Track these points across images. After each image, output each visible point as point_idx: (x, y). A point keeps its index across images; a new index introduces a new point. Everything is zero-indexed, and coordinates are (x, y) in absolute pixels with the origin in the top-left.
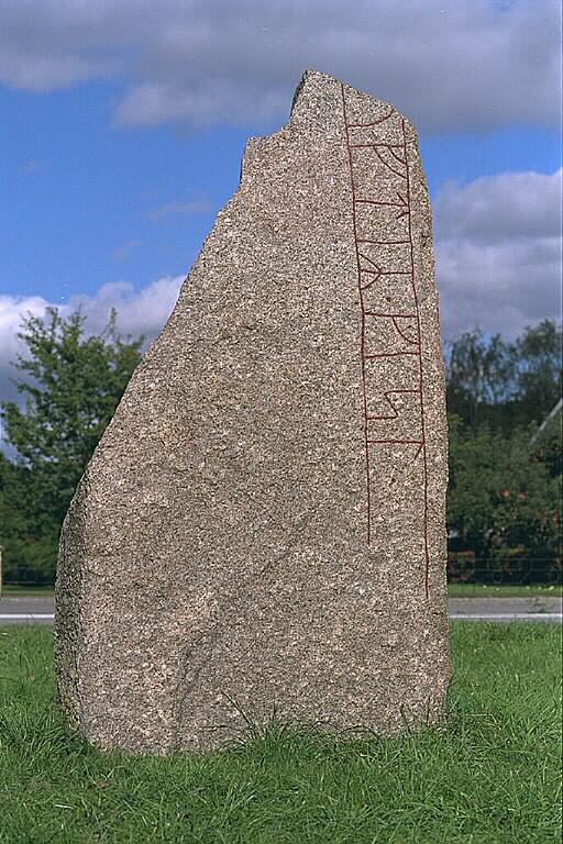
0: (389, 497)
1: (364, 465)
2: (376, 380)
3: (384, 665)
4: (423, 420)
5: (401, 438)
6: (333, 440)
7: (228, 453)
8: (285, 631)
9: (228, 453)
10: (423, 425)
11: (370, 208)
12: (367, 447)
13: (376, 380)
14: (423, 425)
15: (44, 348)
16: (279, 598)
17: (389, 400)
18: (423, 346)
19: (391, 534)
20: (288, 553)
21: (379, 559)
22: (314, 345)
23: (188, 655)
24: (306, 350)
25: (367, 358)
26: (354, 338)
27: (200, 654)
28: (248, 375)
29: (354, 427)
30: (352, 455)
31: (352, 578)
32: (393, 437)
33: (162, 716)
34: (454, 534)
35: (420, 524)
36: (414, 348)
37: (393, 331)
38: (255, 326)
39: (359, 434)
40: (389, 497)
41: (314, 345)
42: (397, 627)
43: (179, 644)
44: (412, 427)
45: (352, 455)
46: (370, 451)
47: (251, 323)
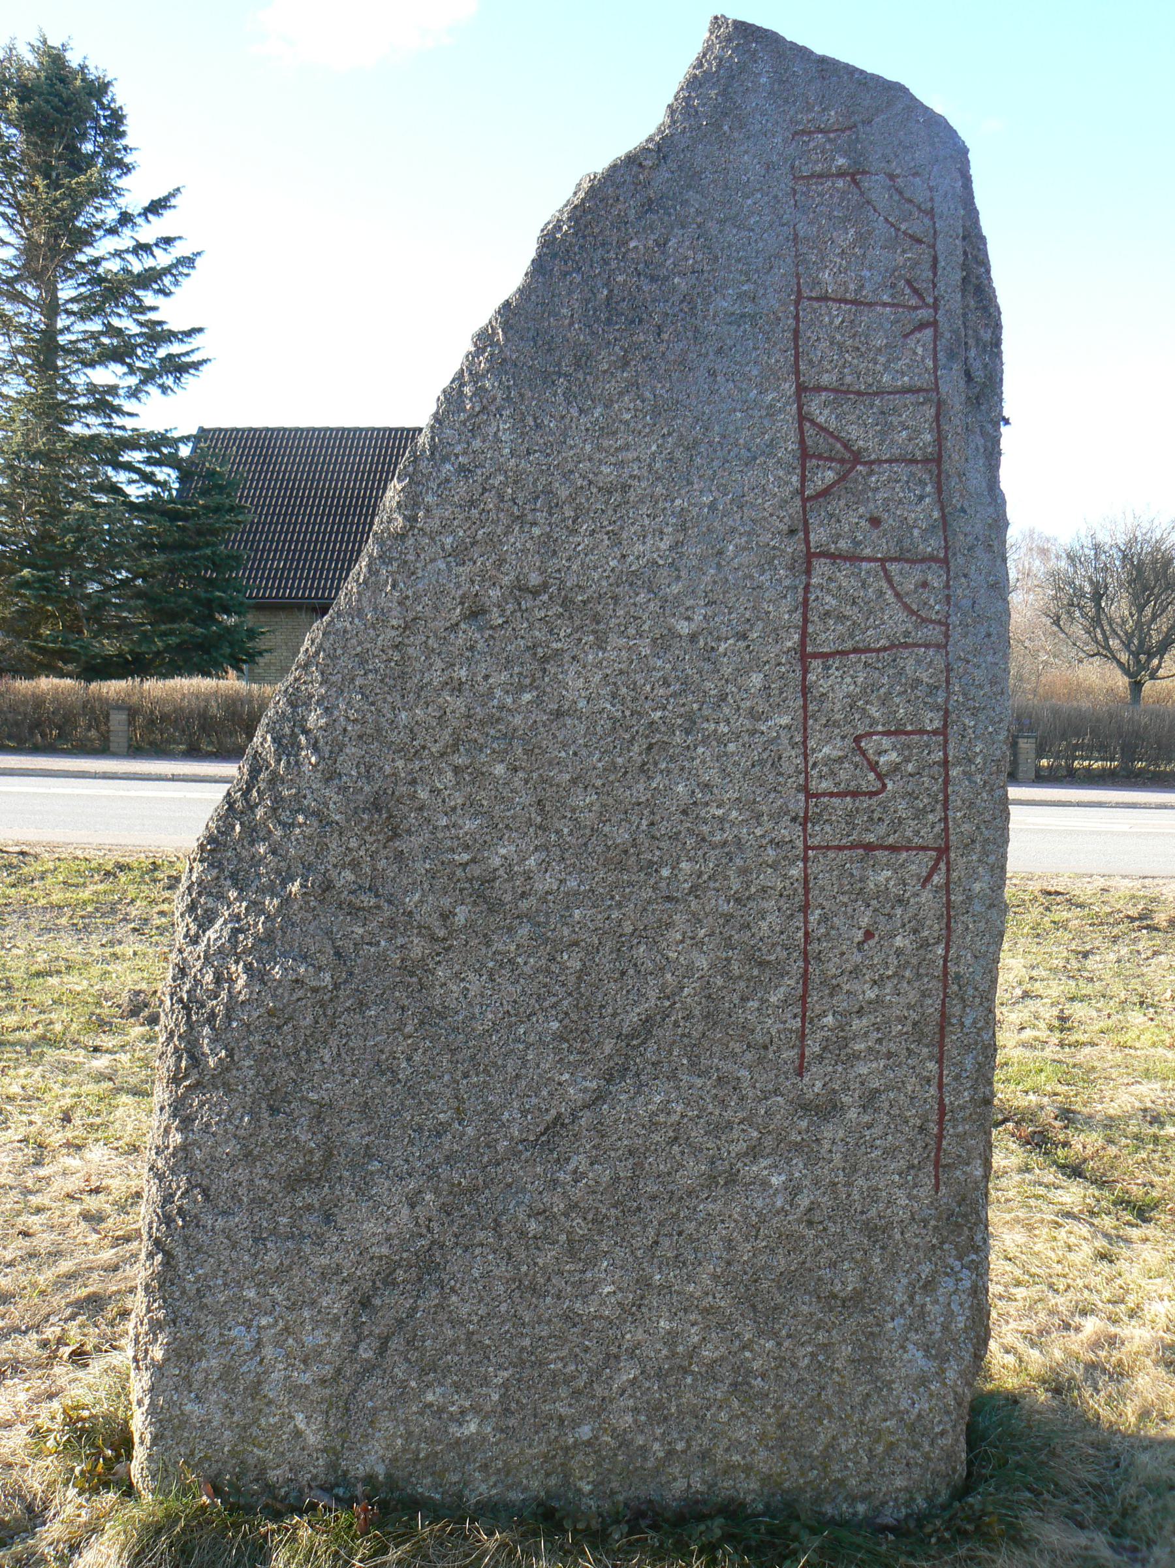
0: (856, 972)
1: (799, 899)
2: (837, 705)
3: (821, 1337)
4: (946, 797)
5: (891, 840)
6: (725, 843)
7: (476, 870)
8: (591, 1262)
9: (476, 870)
10: (946, 808)
11: (836, 314)
12: (805, 859)
13: (837, 705)
14: (946, 808)
15: (1111, 716)
16: (577, 1193)
17: (863, 753)
18: (956, 633)
19: (856, 1056)
20: (599, 1098)
21: (826, 1109)
22: (684, 628)
23: (365, 1303)
24: (664, 642)
25: (815, 656)
26: (784, 612)
27: (394, 1304)
28: (527, 697)
29: (776, 817)
30: (768, 878)
31: (754, 1152)
32: (871, 838)
33: (302, 1426)
34: (983, 1553)
35: (931, 1029)
36: (933, 633)
37: (881, 593)
38: (545, 586)
39: (787, 831)
40: (856, 972)
41: (684, 628)
42: (858, 1256)
43: (344, 1281)
44: (920, 814)
45: (768, 878)
46: (814, 869)
47: (535, 579)
